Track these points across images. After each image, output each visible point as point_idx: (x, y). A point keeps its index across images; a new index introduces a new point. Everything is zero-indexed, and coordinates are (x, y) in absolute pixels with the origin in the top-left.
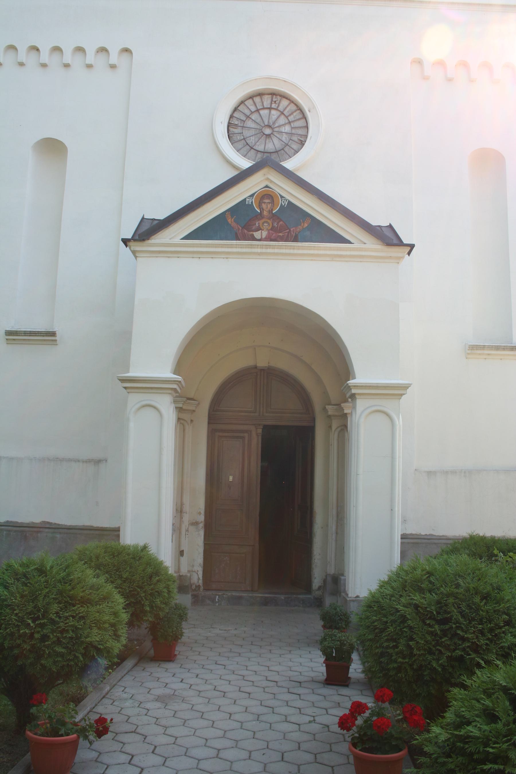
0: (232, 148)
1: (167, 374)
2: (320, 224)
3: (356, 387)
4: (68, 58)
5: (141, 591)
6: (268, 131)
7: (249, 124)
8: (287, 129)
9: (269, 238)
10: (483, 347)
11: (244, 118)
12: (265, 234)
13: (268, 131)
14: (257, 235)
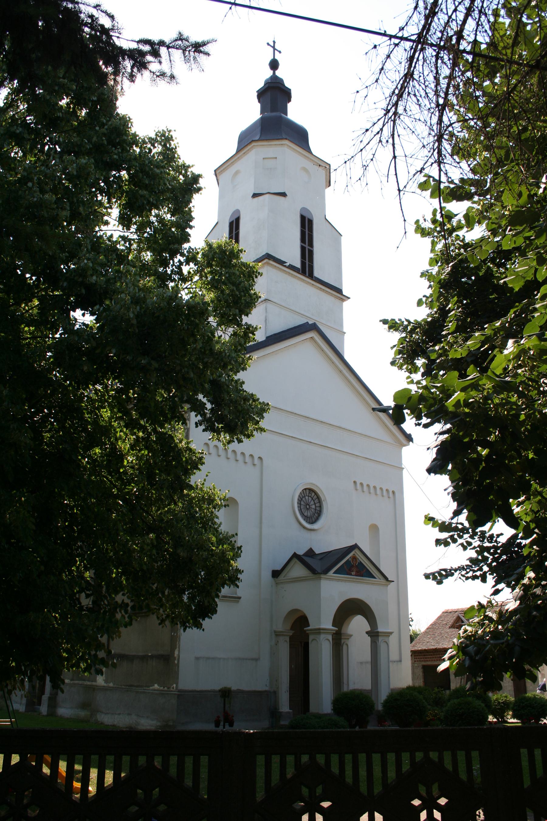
14: (353, 573)
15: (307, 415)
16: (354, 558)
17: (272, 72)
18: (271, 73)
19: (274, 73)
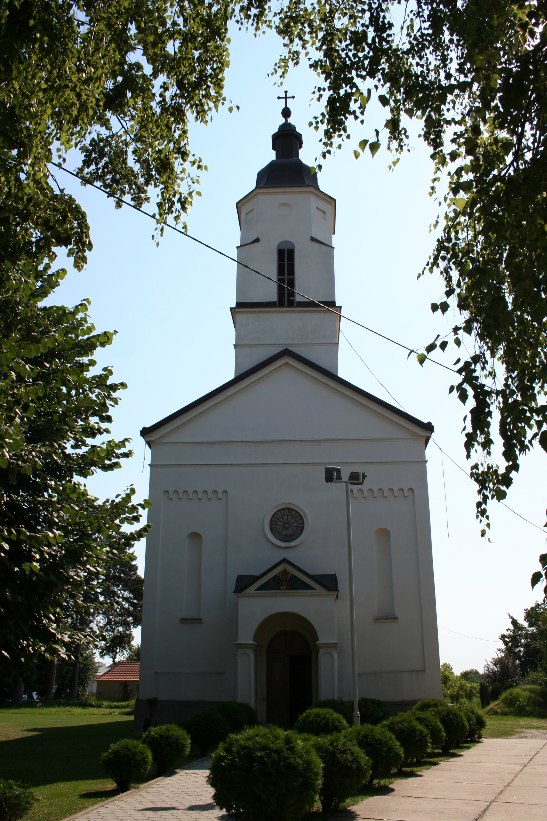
0: (280, 312)
1: (251, 641)
2: (304, 582)
3: (319, 644)
4: (200, 496)
5: (506, 250)
6: (287, 526)
7: (279, 523)
8: (295, 524)
9: (286, 589)
10: (381, 619)
11: (276, 520)
12: (284, 587)
13: (287, 526)
14: (282, 588)
15: (281, 439)
16: (285, 572)
17: (284, 119)
18: (283, 120)
19: (286, 121)
